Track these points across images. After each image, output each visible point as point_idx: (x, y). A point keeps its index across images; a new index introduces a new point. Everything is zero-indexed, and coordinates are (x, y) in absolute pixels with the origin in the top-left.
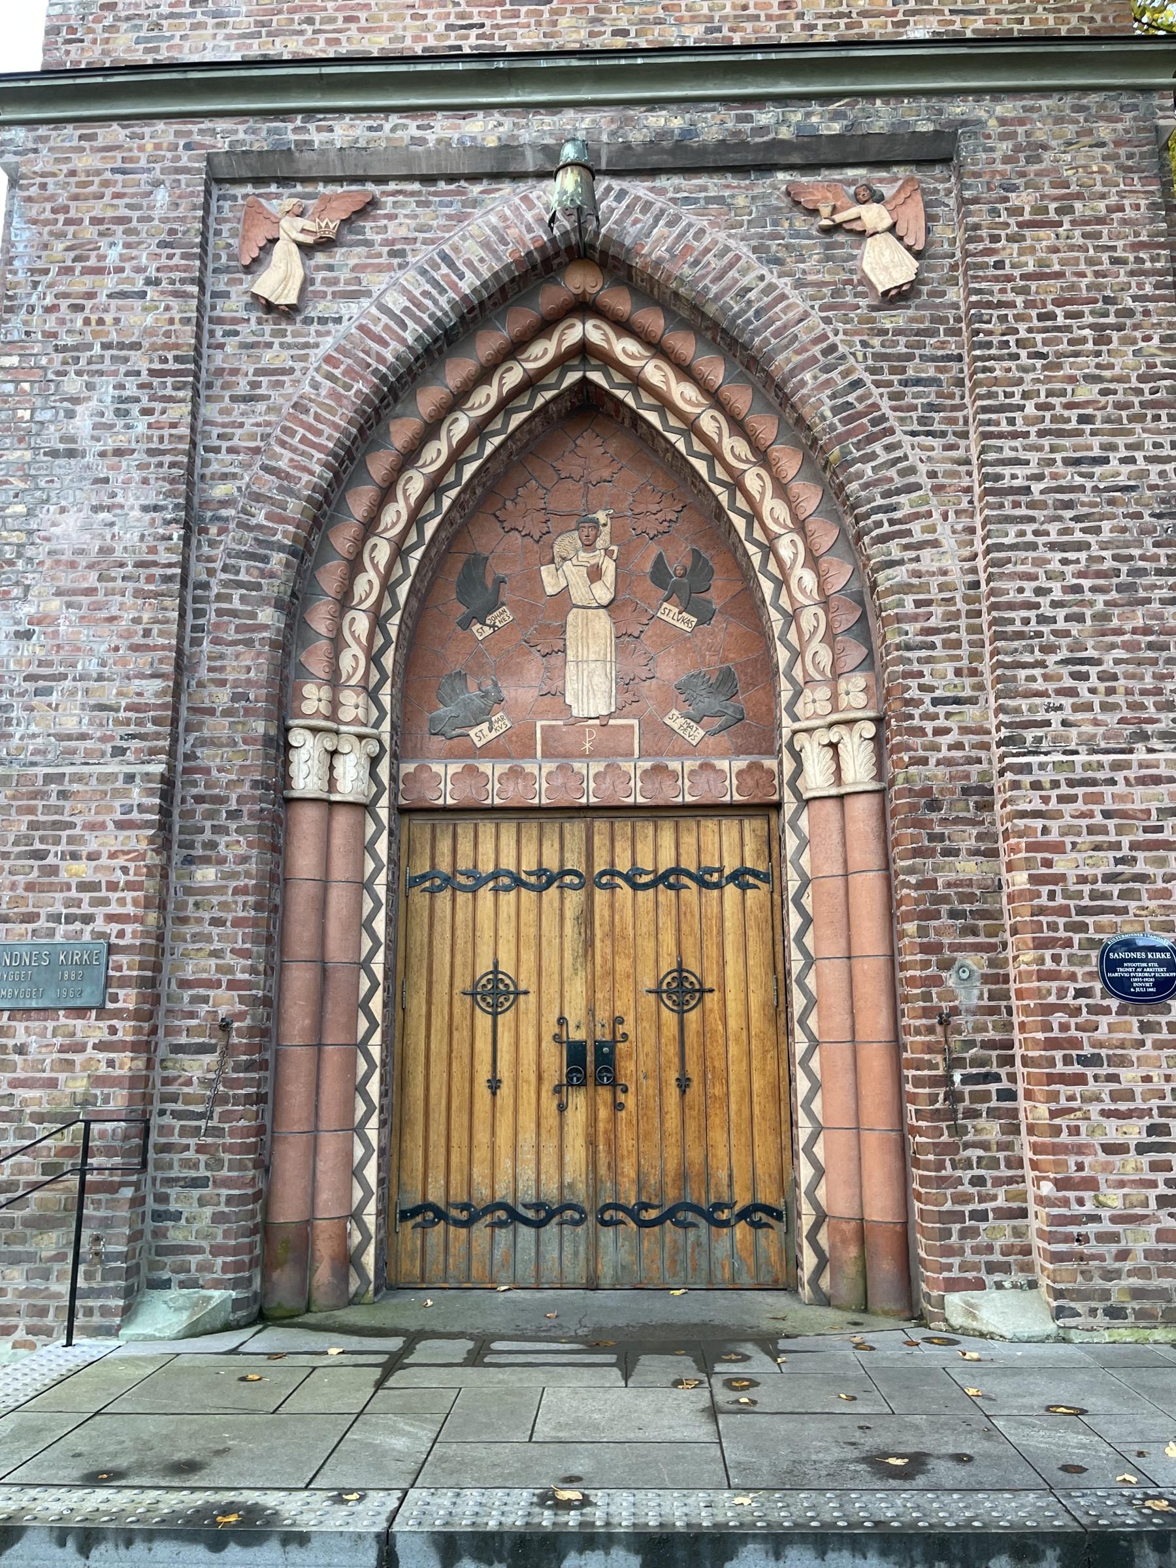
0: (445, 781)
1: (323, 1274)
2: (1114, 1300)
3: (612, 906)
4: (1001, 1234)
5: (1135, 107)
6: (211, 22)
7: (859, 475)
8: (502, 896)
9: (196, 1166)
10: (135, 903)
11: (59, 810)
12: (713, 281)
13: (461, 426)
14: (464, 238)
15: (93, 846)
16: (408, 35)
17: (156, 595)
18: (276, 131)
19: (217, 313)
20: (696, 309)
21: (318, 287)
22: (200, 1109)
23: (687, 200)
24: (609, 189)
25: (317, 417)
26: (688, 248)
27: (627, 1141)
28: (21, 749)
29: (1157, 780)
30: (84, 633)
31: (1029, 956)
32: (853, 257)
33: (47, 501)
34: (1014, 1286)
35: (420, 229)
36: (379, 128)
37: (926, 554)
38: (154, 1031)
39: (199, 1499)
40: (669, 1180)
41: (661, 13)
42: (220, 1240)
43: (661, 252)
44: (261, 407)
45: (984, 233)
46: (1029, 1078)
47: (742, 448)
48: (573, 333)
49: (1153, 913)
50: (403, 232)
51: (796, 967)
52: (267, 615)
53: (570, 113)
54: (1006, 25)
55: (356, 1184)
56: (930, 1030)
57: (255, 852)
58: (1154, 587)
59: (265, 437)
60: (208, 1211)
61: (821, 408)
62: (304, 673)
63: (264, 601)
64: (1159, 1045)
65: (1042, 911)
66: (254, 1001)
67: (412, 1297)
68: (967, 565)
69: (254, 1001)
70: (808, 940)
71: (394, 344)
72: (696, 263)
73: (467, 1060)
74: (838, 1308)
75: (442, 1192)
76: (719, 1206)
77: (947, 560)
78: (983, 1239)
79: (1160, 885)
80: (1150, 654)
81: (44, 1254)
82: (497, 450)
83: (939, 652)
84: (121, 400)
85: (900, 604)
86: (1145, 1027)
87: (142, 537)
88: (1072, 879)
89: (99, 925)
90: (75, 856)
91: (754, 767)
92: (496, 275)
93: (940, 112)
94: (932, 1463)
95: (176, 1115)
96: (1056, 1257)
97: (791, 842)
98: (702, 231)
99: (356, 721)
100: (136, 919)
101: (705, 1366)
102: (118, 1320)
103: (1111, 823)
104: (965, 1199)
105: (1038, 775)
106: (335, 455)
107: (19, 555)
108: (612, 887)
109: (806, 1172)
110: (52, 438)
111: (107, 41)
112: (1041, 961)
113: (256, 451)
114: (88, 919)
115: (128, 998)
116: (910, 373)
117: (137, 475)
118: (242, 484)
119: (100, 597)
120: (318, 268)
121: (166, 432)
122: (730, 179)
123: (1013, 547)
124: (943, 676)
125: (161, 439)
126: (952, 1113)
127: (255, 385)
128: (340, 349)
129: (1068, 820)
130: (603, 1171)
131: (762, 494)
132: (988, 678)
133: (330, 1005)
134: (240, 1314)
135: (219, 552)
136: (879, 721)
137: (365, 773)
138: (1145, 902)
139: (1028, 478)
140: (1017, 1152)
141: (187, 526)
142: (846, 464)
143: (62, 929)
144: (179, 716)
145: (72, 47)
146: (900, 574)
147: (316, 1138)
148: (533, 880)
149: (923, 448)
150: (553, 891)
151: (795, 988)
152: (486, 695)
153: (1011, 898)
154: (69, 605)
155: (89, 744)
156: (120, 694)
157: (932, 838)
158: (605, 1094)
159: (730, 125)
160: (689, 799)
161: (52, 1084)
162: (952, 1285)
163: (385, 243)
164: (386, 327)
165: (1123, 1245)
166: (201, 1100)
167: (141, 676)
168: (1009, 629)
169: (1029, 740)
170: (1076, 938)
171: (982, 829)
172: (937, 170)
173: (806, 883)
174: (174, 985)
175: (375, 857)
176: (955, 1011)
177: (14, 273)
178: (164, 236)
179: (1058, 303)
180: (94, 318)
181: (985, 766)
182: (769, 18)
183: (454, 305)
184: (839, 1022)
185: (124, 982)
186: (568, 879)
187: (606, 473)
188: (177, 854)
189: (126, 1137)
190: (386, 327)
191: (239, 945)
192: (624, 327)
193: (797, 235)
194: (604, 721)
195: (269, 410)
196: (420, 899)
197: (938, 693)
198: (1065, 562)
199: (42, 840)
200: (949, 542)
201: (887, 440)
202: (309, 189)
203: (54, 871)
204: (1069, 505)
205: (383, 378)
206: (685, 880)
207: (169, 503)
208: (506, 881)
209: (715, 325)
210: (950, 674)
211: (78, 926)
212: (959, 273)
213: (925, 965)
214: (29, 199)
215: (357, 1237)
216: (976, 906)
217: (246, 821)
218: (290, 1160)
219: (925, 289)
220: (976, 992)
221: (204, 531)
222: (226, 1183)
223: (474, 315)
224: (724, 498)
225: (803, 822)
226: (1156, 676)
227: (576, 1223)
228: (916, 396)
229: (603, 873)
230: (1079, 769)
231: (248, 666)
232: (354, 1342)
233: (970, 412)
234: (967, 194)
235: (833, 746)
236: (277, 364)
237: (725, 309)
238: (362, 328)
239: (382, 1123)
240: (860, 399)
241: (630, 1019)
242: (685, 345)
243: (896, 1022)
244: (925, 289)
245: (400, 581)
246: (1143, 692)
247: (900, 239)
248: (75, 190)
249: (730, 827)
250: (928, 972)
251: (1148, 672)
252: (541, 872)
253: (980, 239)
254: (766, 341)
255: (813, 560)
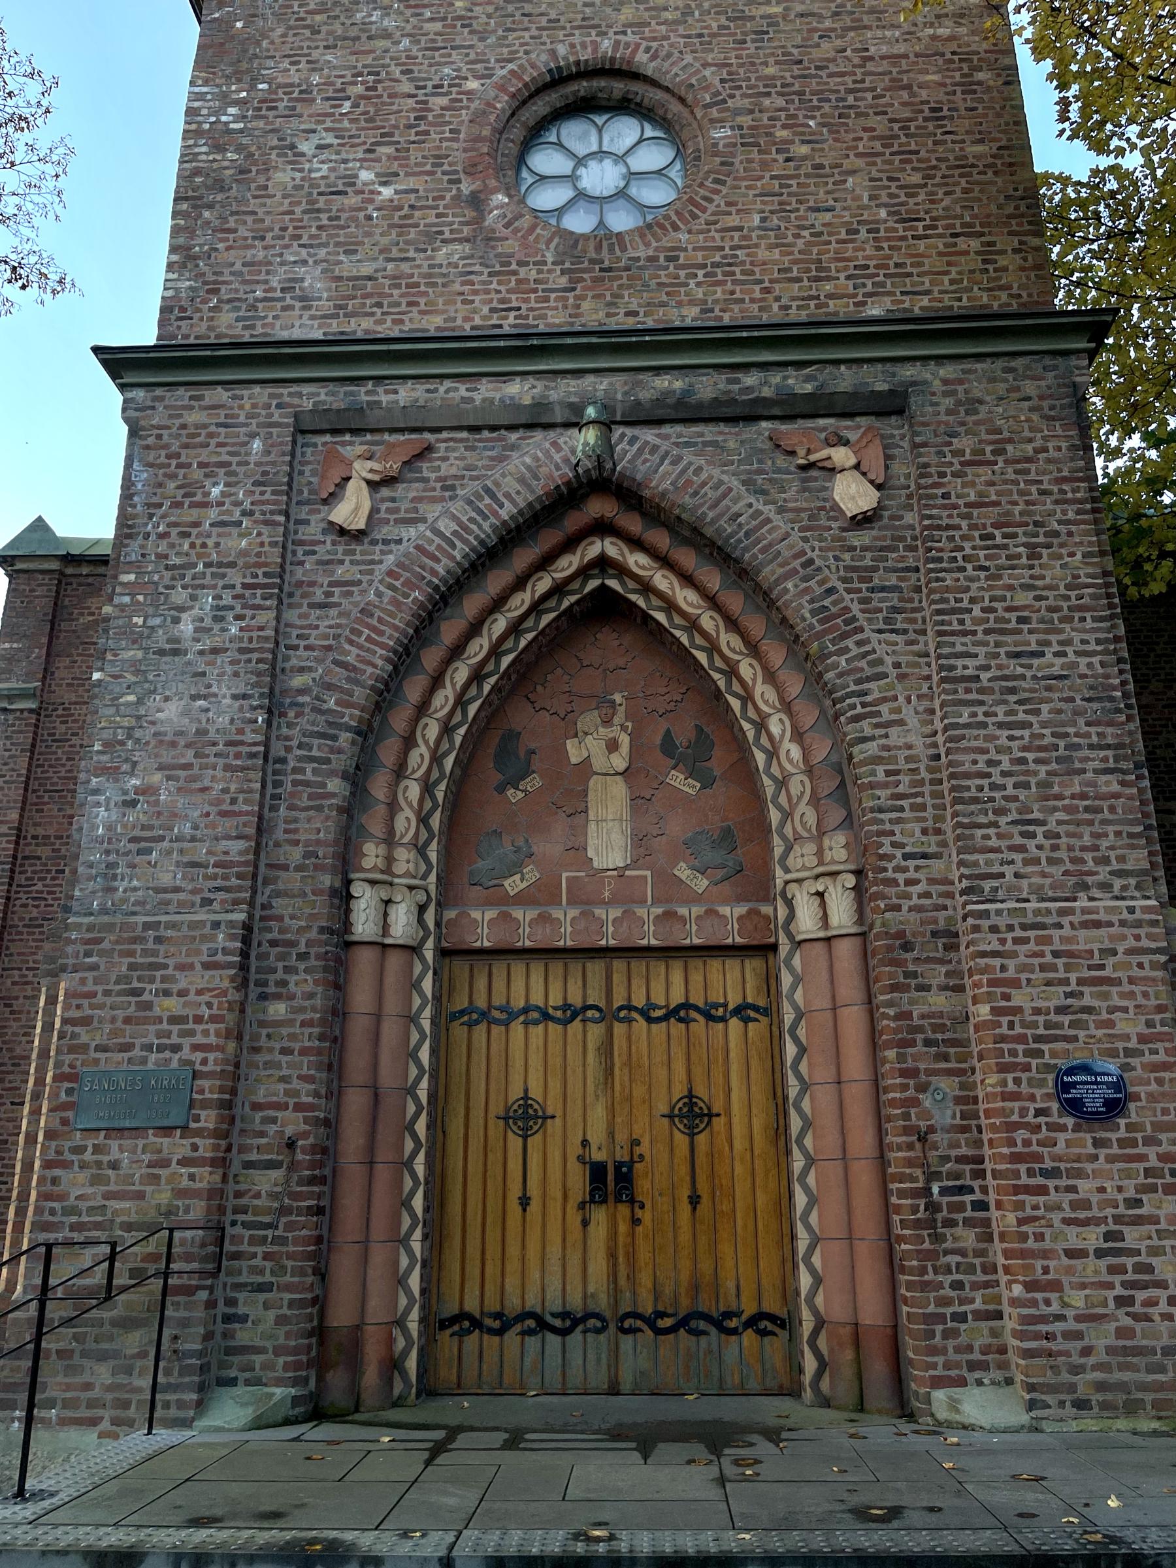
0: (482, 926)
1: (371, 1376)
2: (1081, 1392)
3: (629, 1038)
4: (978, 1334)
5: (1055, 368)
6: (298, 305)
7: (836, 666)
8: (531, 1028)
9: (262, 1272)
10: (217, 1035)
11: (155, 953)
12: (711, 508)
13: (500, 625)
14: (504, 475)
15: (182, 985)
16: (460, 316)
17: (243, 769)
18: (352, 394)
19: (300, 536)
20: (695, 530)
21: (383, 515)
22: (266, 1219)
23: (687, 444)
24: (623, 435)
25: (380, 620)
26: (689, 482)
27: (644, 1254)
28: (124, 901)
29: (1097, 924)
30: (181, 802)
31: (992, 1079)
32: (826, 489)
33: (154, 692)
34: (993, 1383)
35: (468, 468)
36: (436, 390)
37: (894, 731)
38: (229, 1149)
39: (288, 1536)
40: (682, 1290)
41: (665, 298)
42: (281, 1340)
43: (666, 485)
44: (333, 612)
45: (933, 470)
46: (999, 1190)
47: (736, 642)
48: (594, 548)
49: (1100, 1041)
50: (453, 471)
51: (793, 1092)
52: (335, 785)
53: (590, 379)
54: (947, 303)
55: (401, 1293)
56: (910, 1146)
57: (320, 989)
58: (1087, 759)
59: (336, 637)
60: (271, 1315)
61: (802, 612)
62: (364, 833)
63: (332, 773)
64: (1111, 1159)
65: (1003, 1039)
66: (317, 1122)
67: (450, 1402)
68: (929, 740)
69: (317, 1122)
70: (803, 1067)
71: (444, 560)
72: (696, 493)
73: (500, 1179)
74: (837, 1408)
75: (477, 1302)
76: (728, 1315)
77: (912, 735)
78: (963, 1340)
79: (1105, 1016)
80: (1087, 816)
81: (129, 1352)
82: (530, 643)
83: (907, 814)
84: (218, 608)
85: (873, 773)
86: (1097, 1143)
87: (232, 721)
88: (1028, 1011)
89: (186, 1053)
90: (167, 993)
91: (753, 912)
92: (530, 504)
93: (894, 375)
94: (906, 1513)
95: (245, 1225)
96: (1028, 1354)
97: (786, 980)
98: (699, 470)
99: (407, 874)
100: (219, 1048)
101: (716, 1449)
102: (191, 1413)
103: (1060, 962)
104: (947, 1302)
105: (995, 920)
106: (395, 652)
107: (129, 737)
108: (630, 1021)
109: (805, 1281)
110: (160, 640)
111: (212, 319)
112: (1004, 1083)
113: (329, 648)
114: (176, 1048)
115: (208, 1119)
116: (876, 581)
117: (229, 669)
118: (316, 675)
119: (196, 770)
120: (383, 500)
121: (255, 634)
122: (722, 427)
123: (967, 726)
124: (911, 834)
125: (250, 640)
126: (932, 1222)
127: (328, 594)
128: (400, 565)
129: (1022, 959)
130: (622, 1282)
131: (754, 680)
132: (950, 836)
133: (380, 1127)
134: (298, 1410)
135: (295, 732)
136: (858, 873)
137: (414, 919)
138: (1093, 1032)
139: (978, 668)
140: (991, 1259)
141: (270, 712)
142: (824, 657)
143: (153, 1057)
144: (258, 871)
145: (183, 323)
146: (872, 748)
147: (366, 1249)
148: (559, 1014)
149: (888, 643)
150: (577, 1024)
151: (792, 1112)
152: (518, 850)
153: (977, 1028)
154: (169, 778)
155: (182, 896)
156: (209, 852)
157: (907, 975)
158: (623, 1210)
159: (721, 386)
160: (696, 941)
161: (140, 1196)
162: (938, 1382)
163: (439, 479)
164: (439, 547)
165: (1086, 1342)
166: (268, 1211)
167: (228, 837)
168: (966, 795)
169: (987, 890)
170: (1034, 1063)
171: (949, 967)
172: (893, 419)
173: (800, 1016)
174: (247, 1108)
175: (421, 994)
176: (932, 1129)
177: (134, 506)
178: (258, 477)
179: (996, 526)
180: (198, 542)
181: (950, 912)
182: (752, 301)
183: (495, 529)
184: (832, 1139)
185: (205, 1104)
186: (590, 1013)
187: (621, 662)
188: (253, 991)
189: (203, 1245)
190: (439, 547)
191: (305, 1071)
192: (636, 544)
193: (779, 471)
194: (620, 872)
195: (340, 615)
196: (459, 1031)
197: (908, 849)
198: (1011, 738)
199: (140, 979)
200: (913, 722)
201: (858, 637)
202: (377, 437)
203: (148, 1006)
204: (1013, 690)
205: (436, 588)
206: (693, 1014)
207: (255, 692)
208: (535, 1015)
209: (712, 544)
210: (918, 833)
211: (167, 1054)
212: (914, 501)
213: (905, 1088)
214: (148, 447)
215: (401, 1343)
216: (948, 1035)
217: (313, 962)
218: (344, 1265)
219: (886, 514)
220: (949, 1113)
221: (282, 714)
222: (288, 1288)
223: (511, 537)
224: (722, 684)
225: (797, 962)
226: (1092, 835)
227: (598, 1331)
228: (881, 600)
229: (621, 1008)
230: (1030, 914)
231: (318, 828)
232: (402, 1434)
233: (927, 613)
234: (918, 439)
235: (820, 894)
236: (348, 577)
237: (720, 531)
238: (418, 548)
239: (425, 1237)
240: (834, 603)
241: (646, 1142)
242: (687, 558)
243: (881, 1141)
244: (886, 514)
245: (446, 754)
246: (1083, 849)
247: (864, 474)
248: (185, 440)
249: (733, 967)
250: (907, 1094)
251: (1086, 831)
252: (566, 1007)
253: (930, 475)
254: (755, 556)
255: (798, 736)
